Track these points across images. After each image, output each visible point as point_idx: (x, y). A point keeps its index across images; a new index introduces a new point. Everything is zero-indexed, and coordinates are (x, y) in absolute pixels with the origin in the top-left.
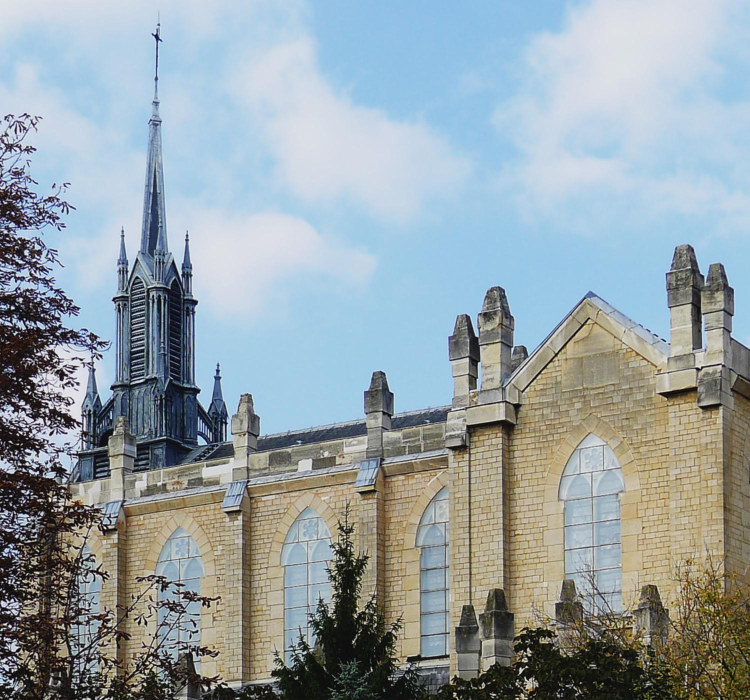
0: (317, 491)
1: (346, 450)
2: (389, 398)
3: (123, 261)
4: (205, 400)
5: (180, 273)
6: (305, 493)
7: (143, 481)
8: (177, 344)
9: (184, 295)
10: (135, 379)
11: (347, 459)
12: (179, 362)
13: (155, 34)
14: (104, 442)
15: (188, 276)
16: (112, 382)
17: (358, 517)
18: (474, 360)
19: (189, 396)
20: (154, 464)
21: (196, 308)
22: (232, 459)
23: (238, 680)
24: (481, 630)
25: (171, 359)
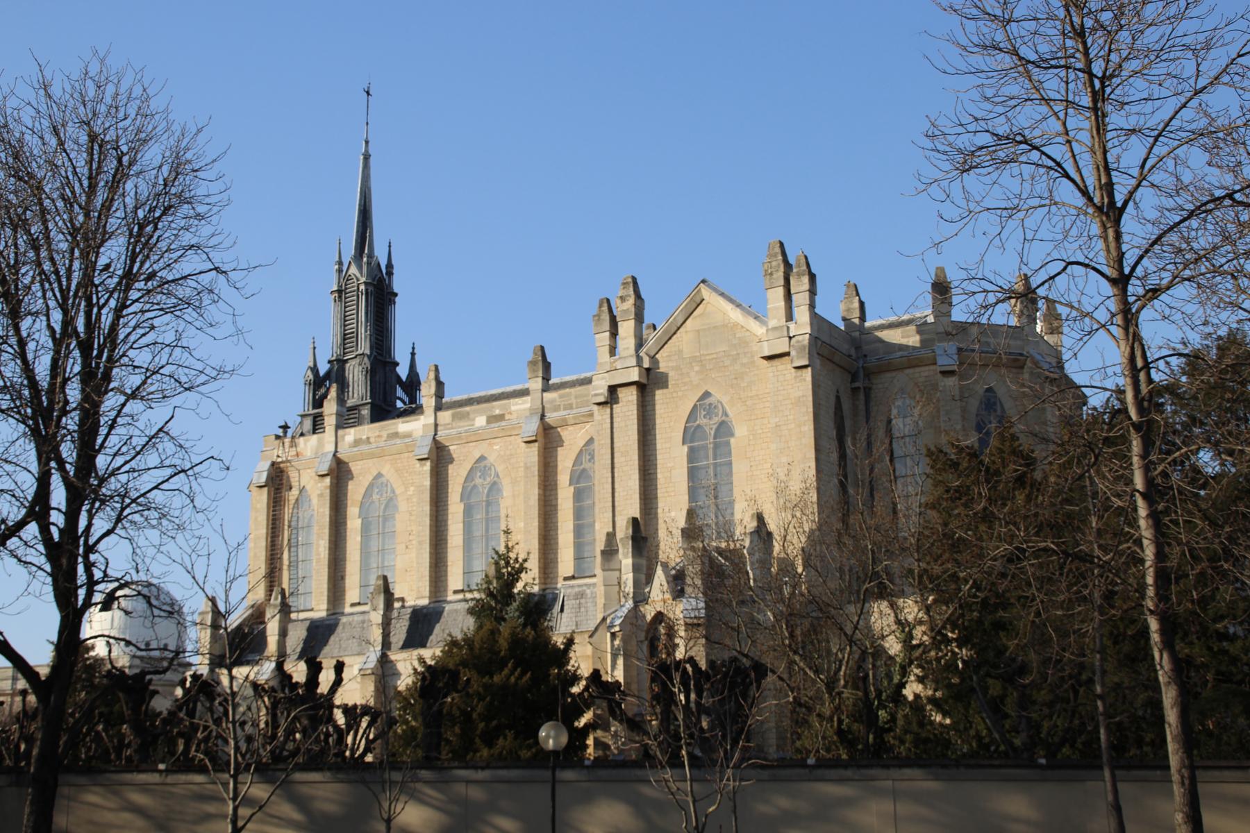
1: (513, 408)
2: (547, 366)
3: (340, 263)
7: (350, 435)
11: (514, 416)
14: (321, 406)
15: (390, 274)
16: (329, 357)
18: (614, 333)
20: (359, 422)
24: (621, 551)
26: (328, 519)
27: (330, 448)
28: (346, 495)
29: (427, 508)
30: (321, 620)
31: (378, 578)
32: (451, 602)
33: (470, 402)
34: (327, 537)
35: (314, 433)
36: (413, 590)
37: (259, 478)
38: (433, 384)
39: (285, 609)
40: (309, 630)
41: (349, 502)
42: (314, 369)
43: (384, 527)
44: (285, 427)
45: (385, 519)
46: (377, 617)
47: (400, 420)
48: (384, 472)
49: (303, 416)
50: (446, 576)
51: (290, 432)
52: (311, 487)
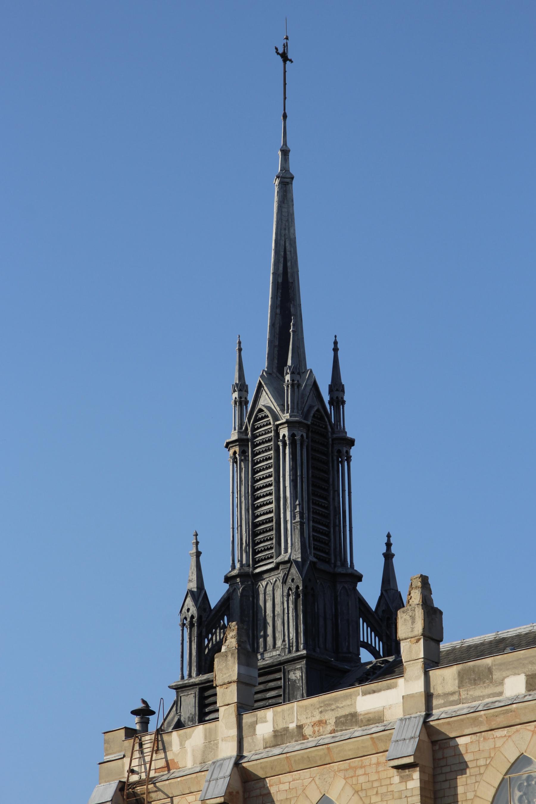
3: (242, 387)
4: (370, 591)
5: (326, 398)
6: (517, 731)
7: (266, 723)
8: (324, 507)
9: (333, 432)
10: (261, 564)
12: (327, 534)
13: (288, 62)
14: (211, 669)
15: (338, 401)
16: (226, 569)
19: (344, 587)
20: (285, 696)
21: (353, 451)
22: (401, 681)
25: (315, 530)
27: (228, 750)
33: (498, 646)
35: (202, 720)
38: (419, 613)
42: (199, 595)
44: (144, 713)
47: (359, 689)
49: (179, 689)
51: (154, 723)
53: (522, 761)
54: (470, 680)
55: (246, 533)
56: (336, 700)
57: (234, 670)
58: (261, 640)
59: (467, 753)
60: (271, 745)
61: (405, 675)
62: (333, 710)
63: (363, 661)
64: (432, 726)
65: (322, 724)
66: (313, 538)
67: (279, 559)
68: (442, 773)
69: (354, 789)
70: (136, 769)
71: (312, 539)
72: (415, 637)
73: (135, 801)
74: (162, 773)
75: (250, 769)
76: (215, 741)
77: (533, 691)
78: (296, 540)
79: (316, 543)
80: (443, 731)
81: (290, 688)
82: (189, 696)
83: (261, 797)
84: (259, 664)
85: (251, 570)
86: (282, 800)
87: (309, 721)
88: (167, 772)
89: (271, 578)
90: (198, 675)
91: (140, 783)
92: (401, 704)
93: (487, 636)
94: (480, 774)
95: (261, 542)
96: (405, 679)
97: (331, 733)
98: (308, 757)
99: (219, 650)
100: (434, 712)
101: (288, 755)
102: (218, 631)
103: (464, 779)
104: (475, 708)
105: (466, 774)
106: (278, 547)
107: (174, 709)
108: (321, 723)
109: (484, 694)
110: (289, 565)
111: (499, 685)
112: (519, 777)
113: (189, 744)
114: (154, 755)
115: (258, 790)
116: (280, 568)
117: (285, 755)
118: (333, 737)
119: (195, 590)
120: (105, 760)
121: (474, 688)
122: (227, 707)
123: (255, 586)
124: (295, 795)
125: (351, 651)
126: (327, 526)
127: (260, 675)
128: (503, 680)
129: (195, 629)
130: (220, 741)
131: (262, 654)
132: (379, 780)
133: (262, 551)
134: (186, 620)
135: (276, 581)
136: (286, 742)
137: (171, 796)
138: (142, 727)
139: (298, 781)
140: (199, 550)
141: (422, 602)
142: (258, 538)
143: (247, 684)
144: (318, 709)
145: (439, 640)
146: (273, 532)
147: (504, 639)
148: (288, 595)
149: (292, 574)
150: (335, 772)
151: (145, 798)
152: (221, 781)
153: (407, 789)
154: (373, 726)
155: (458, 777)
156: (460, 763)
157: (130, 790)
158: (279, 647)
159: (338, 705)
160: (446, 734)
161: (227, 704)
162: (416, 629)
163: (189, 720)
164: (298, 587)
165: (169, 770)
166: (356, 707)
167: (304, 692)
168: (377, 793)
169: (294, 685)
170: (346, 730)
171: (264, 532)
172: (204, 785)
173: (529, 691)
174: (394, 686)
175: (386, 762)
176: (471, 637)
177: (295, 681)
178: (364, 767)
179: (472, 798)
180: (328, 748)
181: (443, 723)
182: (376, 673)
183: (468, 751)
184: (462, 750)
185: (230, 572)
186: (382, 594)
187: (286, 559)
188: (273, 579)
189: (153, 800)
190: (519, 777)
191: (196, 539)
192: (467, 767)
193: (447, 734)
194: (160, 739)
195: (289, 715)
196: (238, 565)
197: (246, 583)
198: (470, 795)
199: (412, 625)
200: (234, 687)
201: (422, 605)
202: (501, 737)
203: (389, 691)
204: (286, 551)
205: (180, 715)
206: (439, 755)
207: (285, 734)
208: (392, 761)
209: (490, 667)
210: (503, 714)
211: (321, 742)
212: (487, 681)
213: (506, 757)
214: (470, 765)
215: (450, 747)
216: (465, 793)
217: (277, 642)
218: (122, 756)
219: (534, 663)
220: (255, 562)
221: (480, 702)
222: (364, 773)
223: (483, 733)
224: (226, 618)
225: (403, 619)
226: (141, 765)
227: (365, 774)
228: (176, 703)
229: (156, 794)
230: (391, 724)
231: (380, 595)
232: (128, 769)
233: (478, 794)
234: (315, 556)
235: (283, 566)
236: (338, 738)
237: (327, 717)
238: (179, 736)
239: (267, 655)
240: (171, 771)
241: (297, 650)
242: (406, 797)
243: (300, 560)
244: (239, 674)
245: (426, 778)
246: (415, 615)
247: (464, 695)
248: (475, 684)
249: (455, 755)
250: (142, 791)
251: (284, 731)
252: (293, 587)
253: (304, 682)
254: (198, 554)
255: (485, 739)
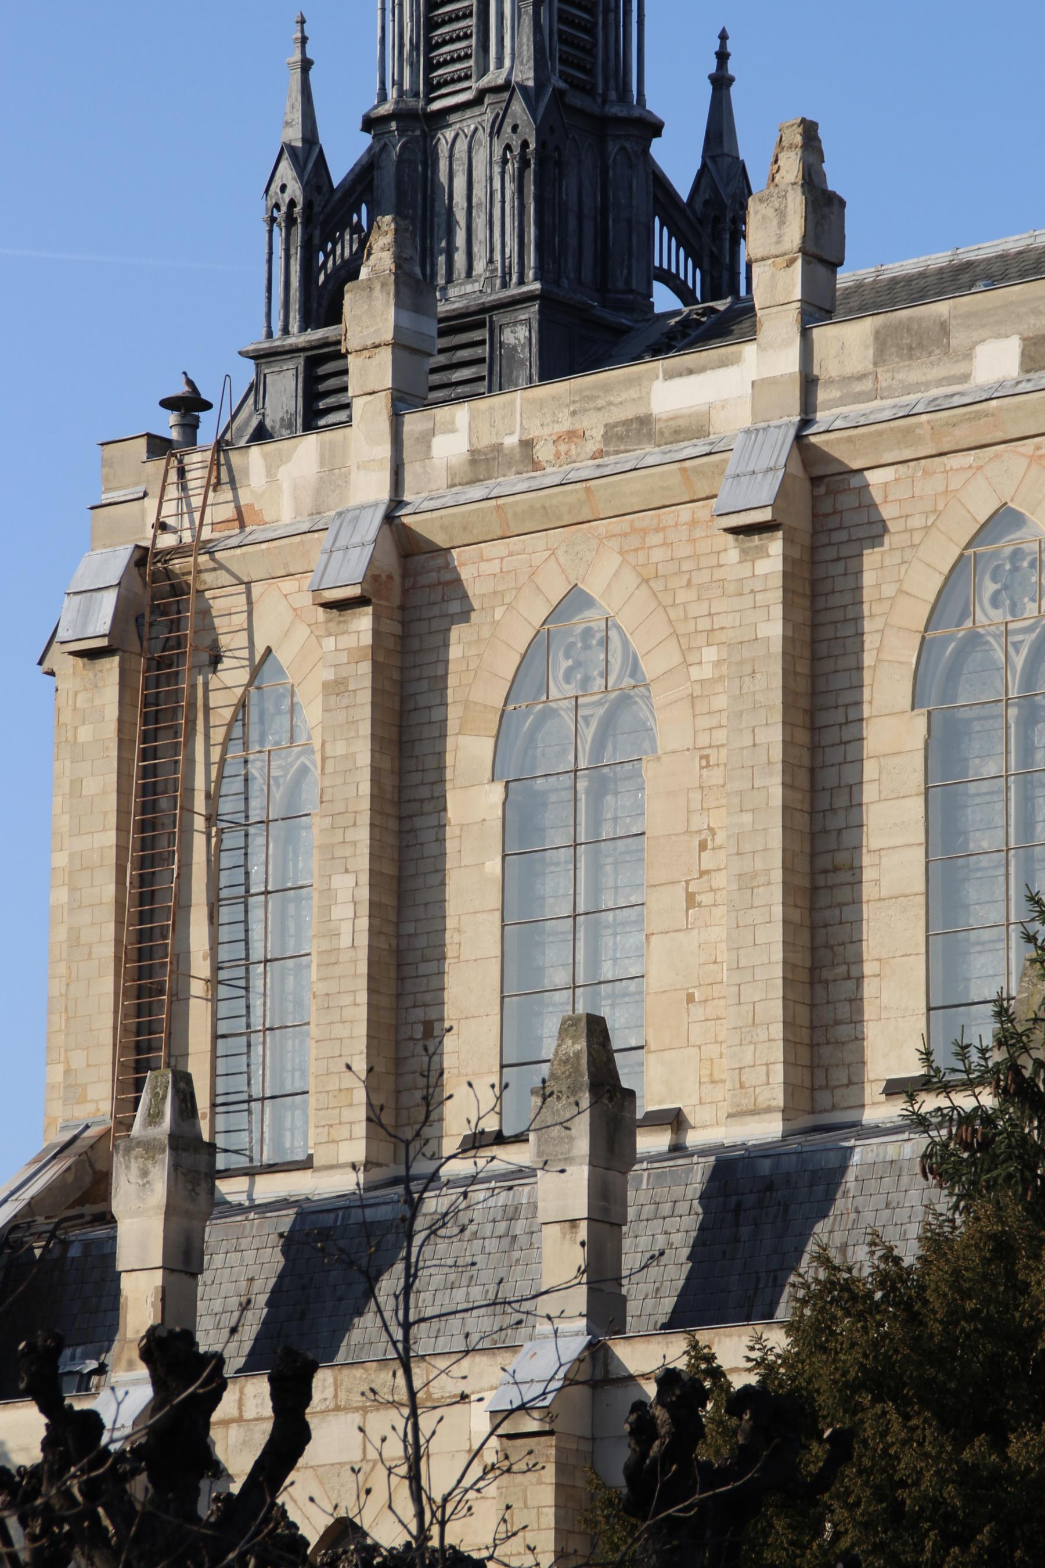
0: (1038, 448)
4: (678, 159)
6: (997, 456)
7: (453, 432)
10: (444, 91)
14: (334, 316)
16: (367, 102)
17: (723, 851)
19: (623, 148)
20: (493, 379)
22: (749, 350)
23: (768, 1110)
25: (564, 18)
26: (365, 788)
27: (372, 488)
28: (440, 683)
29: (773, 737)
30: (338, 1208)
31: (568, 1026)
32: (877, 1131)
33: (958, 279)
34: (363, 862)
35: (310, 424)
36: (716, 1079)
37: (86, 614)
38: (796, 204)
39: (194, 1164)
40: (292, 1244)
41: (454, 714)
42: (307, 156)
43: (596, 820)
44: (189, 405)
45: (600, 791)
46: (566, 1191)
47: (659, 366)
48: (593, 588)
49: (261, 357)
50: (857, 1020)
51: (209, 428)
52: (298, 657)
53: (1004, 519)
54: (900, 348)
55: (412, 21)
56: (607, 388)
57: (386, 319)
58: (442, 259)
59: (886, 502)
60: (465, 481)
61: (759, 337)
62: (599, 409)
63: (658, 309)
64: (813, 445)
65: (575, 439)
66: (560, 37)
67: (485, 82)
68: (830, 544)
69: (639, 574)
70: (171, 521)
71: (556, 38)
72: (785, 254)
73: (168, 588)
74: (227, 533)
75: (418, 529)
76: (343, 470)
77: (1036, 371)
78: (525, 40)
79: (565, 48)
80: (837, 455)
81: (504, 362)
82: (282, 374)
83: (441, 587)
84: (439, 309)
85: (421, 103)
86: (484, 595)
87: (546, 431)
88: (237, 531)
89: (465, 124)
90: (303, 329)
91: (180, 551)
92: (749, 399)
93: (933, 256)
94: (912, 546)
95: (445, 43)
96: (759, 345)
97: (593, 458)
98: (544, 507)
99: (354, 275)
100: (819, 415)
101: (501, 501)
102: (347, 237)
103: (878, 557)
104: (909, 408)
105: (882, 545)
106: (481, 54)
107: (251, 400)
108: (572, 435)
109: (929, 377)
110: (506, 95)
111: (963, 359)
112: (996, 554)
113: (286, 474)
114: (211, 494)
115: (434, 574)
116: (486, 101)
117: (493, 502)
118: (599, 466)
119: (299, 144)
120: (104, 502)
121: (909, 365)
122: (369, 398)
123: (429, 140)
124: (513, 585)
125: (634, 287)
126: (591, 11)
127: (442, 333)
128: (972, 348)
129: (298, 231)
130: (354, 469)
131: (444, 289)
132: (695, 556)
133: (446, 63)
134: (279, 210)
135: (476, 129)
136: (495, 475)
137: (246, 580)
138: (184, 434)
139: (519, 557)
140: (309, 56)
141: (804, 178)
142: (439, 32)
143: (414, 351)
144: (568, 406)
145: (834, 264)
146: (473, 21)
147: (969, 265)
148: (505, 161)
149: (514, 115)
150: (601, 540)
151: (191, 583)
152: (354, 553)
153: (754, 576)
154: (685, 444)
155: (865, 552)
156: (870, 523)
157: (159, 565)
158: (480, 276)
159: (612, 399)
160: (841, 463)
161: (369, 390)
162: (787, 238)
163: (281, 426)
164: (525, 144)
165: (242, 526)
166: (649, 403)
167: (534, 371)
168: (689, 584)
169: (513, 357)
170: (627, 451)
171: (451, 21)
172: (318, 560)
173: (1028, 371)
174: (736, 360)
175: (712, 521)
176: (897, 261)
177: (514, 348)
178: (664, 529)
179: (893, 594)
180: (588, 489)
181: (838, 441)
182: (690, 335)
183: (889, 499)
184: (877, 495)
185: (376, 107)
186: (704, 165)
187: (501, 81)
188: (469, 126)
189: (207, 587)
190: (996, 554)
191: (302, 31)
192: (885, 530)
193: (846, 462)
194: (222, 461)
195: (503, 418)
196: (392, 93)
197: (410, 133)
198: (888, 590)
199: (780, 228)
200: (386, 356)
201: (802, 186)
202: (961, 468)
203: (722, 372)
204: (500, 65)
205: (263, 415)
206: (826, 507)
207: (494, 458)
208: (725, 517)
209: (945, 321)
210: (969, 420)
211: (573, 476)
212: (937, 352)
213: (969, 511)
214: (890, 525)
215: (850, 489)
216: (878, 585)
217: (475, 264)
218: (141, 495)
219: (1041, 313)
220: (431, 87)
221: (919, 395)
222: (662, 542)
223: (923, 461)
224: (364, 208)
225: (759, 216)
226: (182, 515)
227: (664, 544)
228: (253, 387)
229: (213, 574)
230: (725, 441)
231: (699, 167)
232: (153, 520)
233: (906, 587)
234: (563, 75)
235: (492, 96)
236: (610, 467)
237: (585, 424)
238: (265, 456)
239: (453, 292)
240: (248, 529)
241: (521, 282)
242: (752, 591)
243: (531, 83)
244: (396, 327)
245: (797, 553)
246: (786, 207)
247: (885, 379)
248: (911, 358)
249: (859, 507)
250: (185, 567)
251: (492, 451)
252: (516, 143)
253: (534, 349)
254: (306, 65)
255: (925, 472)
